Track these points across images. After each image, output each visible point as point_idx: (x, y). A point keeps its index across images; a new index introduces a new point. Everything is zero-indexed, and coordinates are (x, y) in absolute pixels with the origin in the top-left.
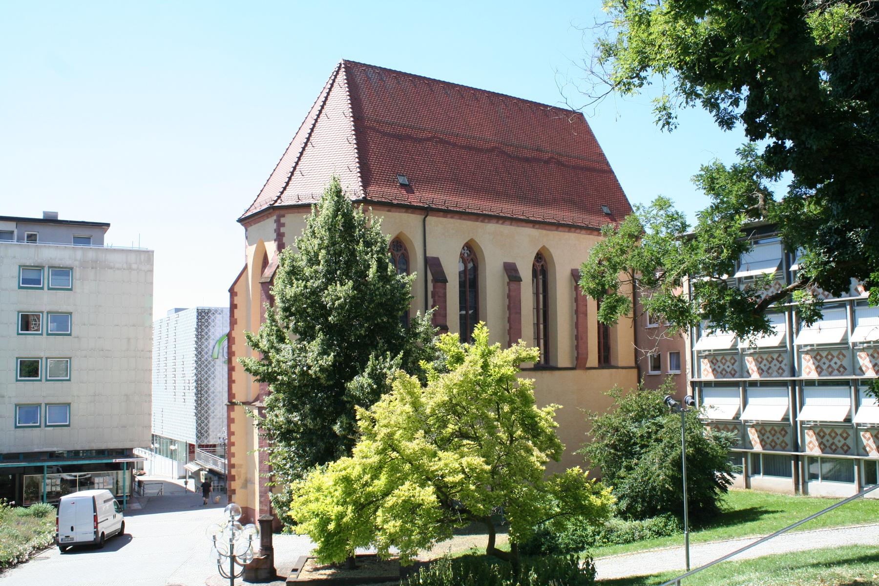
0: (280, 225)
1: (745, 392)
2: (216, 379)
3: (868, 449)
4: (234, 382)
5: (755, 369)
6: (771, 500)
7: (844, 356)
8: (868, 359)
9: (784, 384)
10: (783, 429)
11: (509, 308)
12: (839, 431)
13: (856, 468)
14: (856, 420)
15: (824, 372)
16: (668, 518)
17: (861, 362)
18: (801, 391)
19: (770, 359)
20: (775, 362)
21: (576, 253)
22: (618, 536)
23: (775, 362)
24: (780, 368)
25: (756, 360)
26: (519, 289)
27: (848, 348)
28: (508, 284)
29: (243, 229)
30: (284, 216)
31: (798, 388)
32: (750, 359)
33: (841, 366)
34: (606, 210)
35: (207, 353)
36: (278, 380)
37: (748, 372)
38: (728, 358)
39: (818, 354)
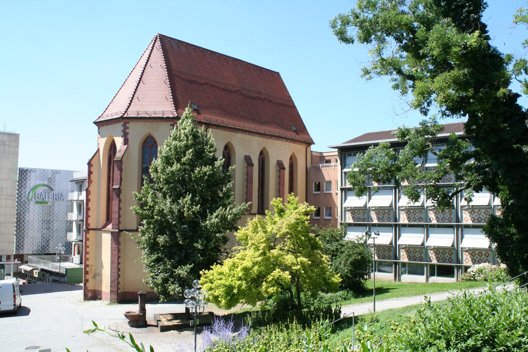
0: (125, 128)
1: (427, 230)
2: (30, 213)
3: (432, 259)
4: (89, 217)
5: (376, 218)
6: (386, 284)
7: (422, 213)
8: (433, 214)
9: (390, 226)
10: (389, 249)
11: (247, 180)
12: (418, 250)
13: (425, 268)
14: (427, 244)
15: (412, 220)
16: (348, 291)
17: (430, 216)
18: (399, 230)
19: (384, 213)
20: (386, 214)
21: (280, 151)
22: (326, 300)
23: (386, 214)
24: (389, 217)
25: (376, 213)
26: (252, 170)
27: (424, 208)
28: (247, 167)
29: (96, 128)
30: (128, 123)
31: (398, 228)
32: (373, 212)
33: (420, 217)
34: (294, 128)
35: (24, 196)
36: (154, 218)
37: (372, 219)
38: (361, 211)
39: (409, 211)
